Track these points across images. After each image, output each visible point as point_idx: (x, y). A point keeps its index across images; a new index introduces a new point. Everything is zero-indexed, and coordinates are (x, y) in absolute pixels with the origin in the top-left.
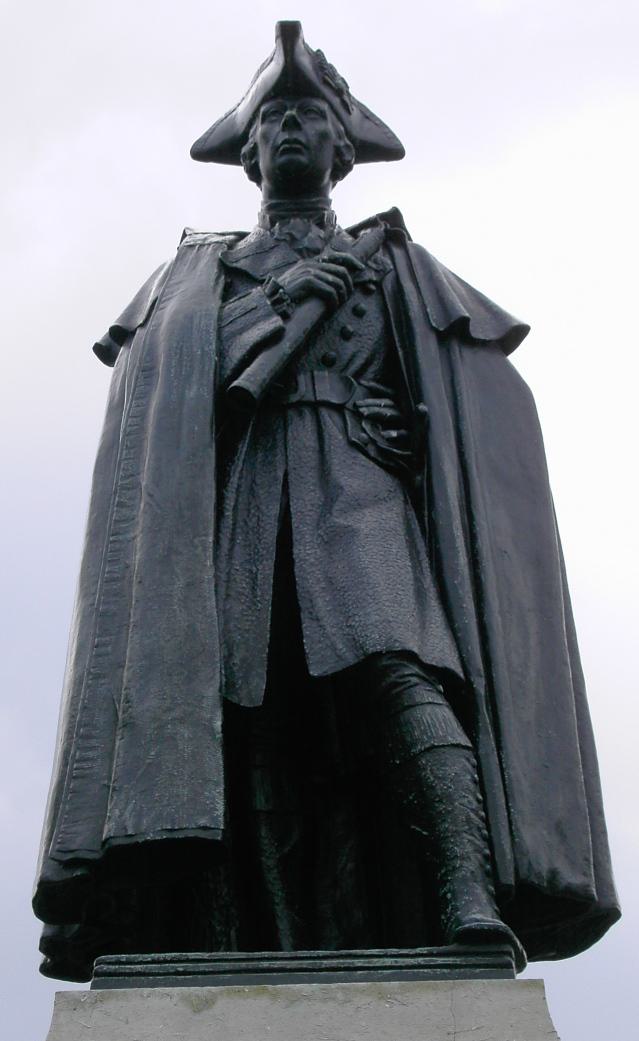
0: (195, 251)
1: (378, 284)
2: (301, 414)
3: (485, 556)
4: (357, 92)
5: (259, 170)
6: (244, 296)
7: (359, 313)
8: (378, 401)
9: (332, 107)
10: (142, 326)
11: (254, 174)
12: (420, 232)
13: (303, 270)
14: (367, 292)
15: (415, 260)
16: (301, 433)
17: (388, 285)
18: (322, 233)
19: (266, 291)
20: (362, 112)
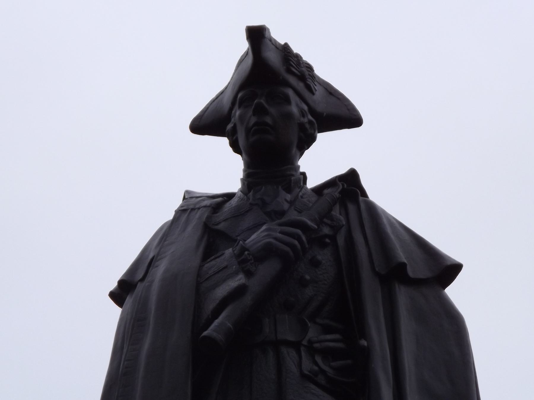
0: (186, 215)
1: (333, 238)
4: (320, 72)
5: (239, 146)
6: (219, 257)
7: (315, 264)
8: (329, 337)
10: (142, 280)
12: (366, 182)
13: (266, 233)
14: (324, 245)
15: (365, 215)
17: (341, 240)
18: (289, 197)
19: (235, 252)
20: (326, 89)
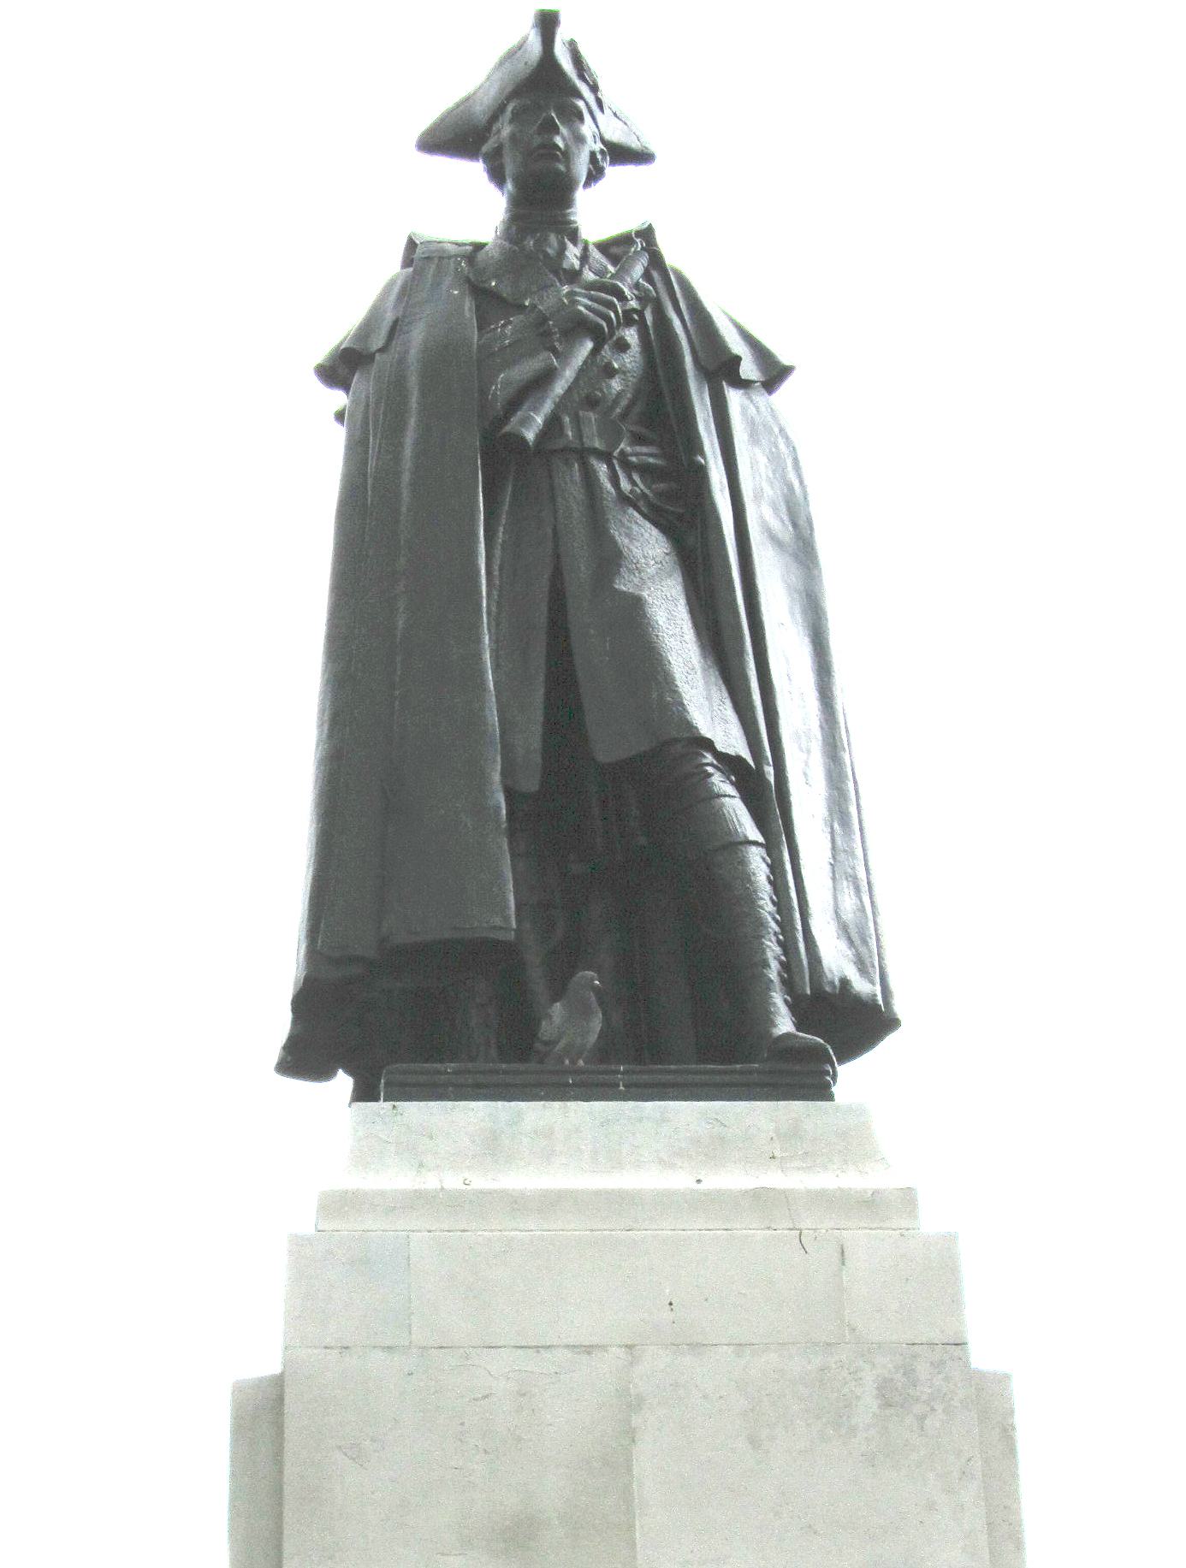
1: (641, 313)
2: (567, 463)
3: (694, 645)
9: (587, 104)
10: (381, 350)
11: (497, 175)
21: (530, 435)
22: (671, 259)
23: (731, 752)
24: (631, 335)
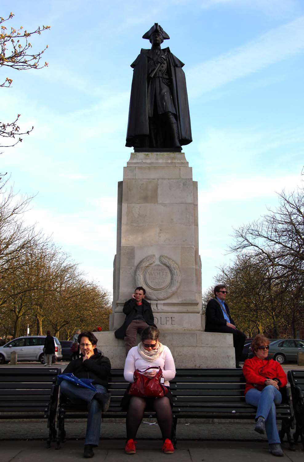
1: (167, 59)
16: (157, 81)
21: (152, 76)
22: (171, 51)
23: (173, 112)
24: (165, 62)
